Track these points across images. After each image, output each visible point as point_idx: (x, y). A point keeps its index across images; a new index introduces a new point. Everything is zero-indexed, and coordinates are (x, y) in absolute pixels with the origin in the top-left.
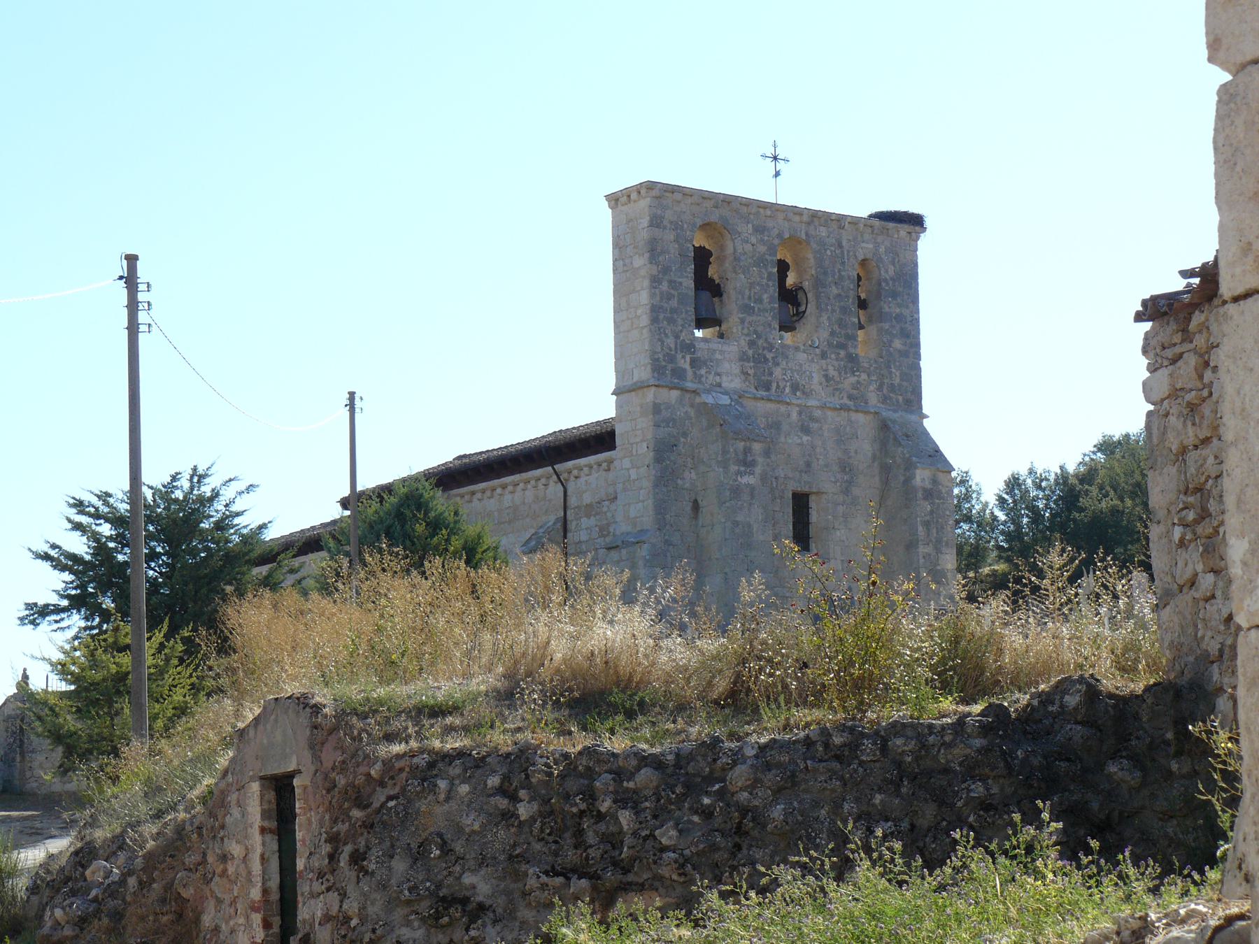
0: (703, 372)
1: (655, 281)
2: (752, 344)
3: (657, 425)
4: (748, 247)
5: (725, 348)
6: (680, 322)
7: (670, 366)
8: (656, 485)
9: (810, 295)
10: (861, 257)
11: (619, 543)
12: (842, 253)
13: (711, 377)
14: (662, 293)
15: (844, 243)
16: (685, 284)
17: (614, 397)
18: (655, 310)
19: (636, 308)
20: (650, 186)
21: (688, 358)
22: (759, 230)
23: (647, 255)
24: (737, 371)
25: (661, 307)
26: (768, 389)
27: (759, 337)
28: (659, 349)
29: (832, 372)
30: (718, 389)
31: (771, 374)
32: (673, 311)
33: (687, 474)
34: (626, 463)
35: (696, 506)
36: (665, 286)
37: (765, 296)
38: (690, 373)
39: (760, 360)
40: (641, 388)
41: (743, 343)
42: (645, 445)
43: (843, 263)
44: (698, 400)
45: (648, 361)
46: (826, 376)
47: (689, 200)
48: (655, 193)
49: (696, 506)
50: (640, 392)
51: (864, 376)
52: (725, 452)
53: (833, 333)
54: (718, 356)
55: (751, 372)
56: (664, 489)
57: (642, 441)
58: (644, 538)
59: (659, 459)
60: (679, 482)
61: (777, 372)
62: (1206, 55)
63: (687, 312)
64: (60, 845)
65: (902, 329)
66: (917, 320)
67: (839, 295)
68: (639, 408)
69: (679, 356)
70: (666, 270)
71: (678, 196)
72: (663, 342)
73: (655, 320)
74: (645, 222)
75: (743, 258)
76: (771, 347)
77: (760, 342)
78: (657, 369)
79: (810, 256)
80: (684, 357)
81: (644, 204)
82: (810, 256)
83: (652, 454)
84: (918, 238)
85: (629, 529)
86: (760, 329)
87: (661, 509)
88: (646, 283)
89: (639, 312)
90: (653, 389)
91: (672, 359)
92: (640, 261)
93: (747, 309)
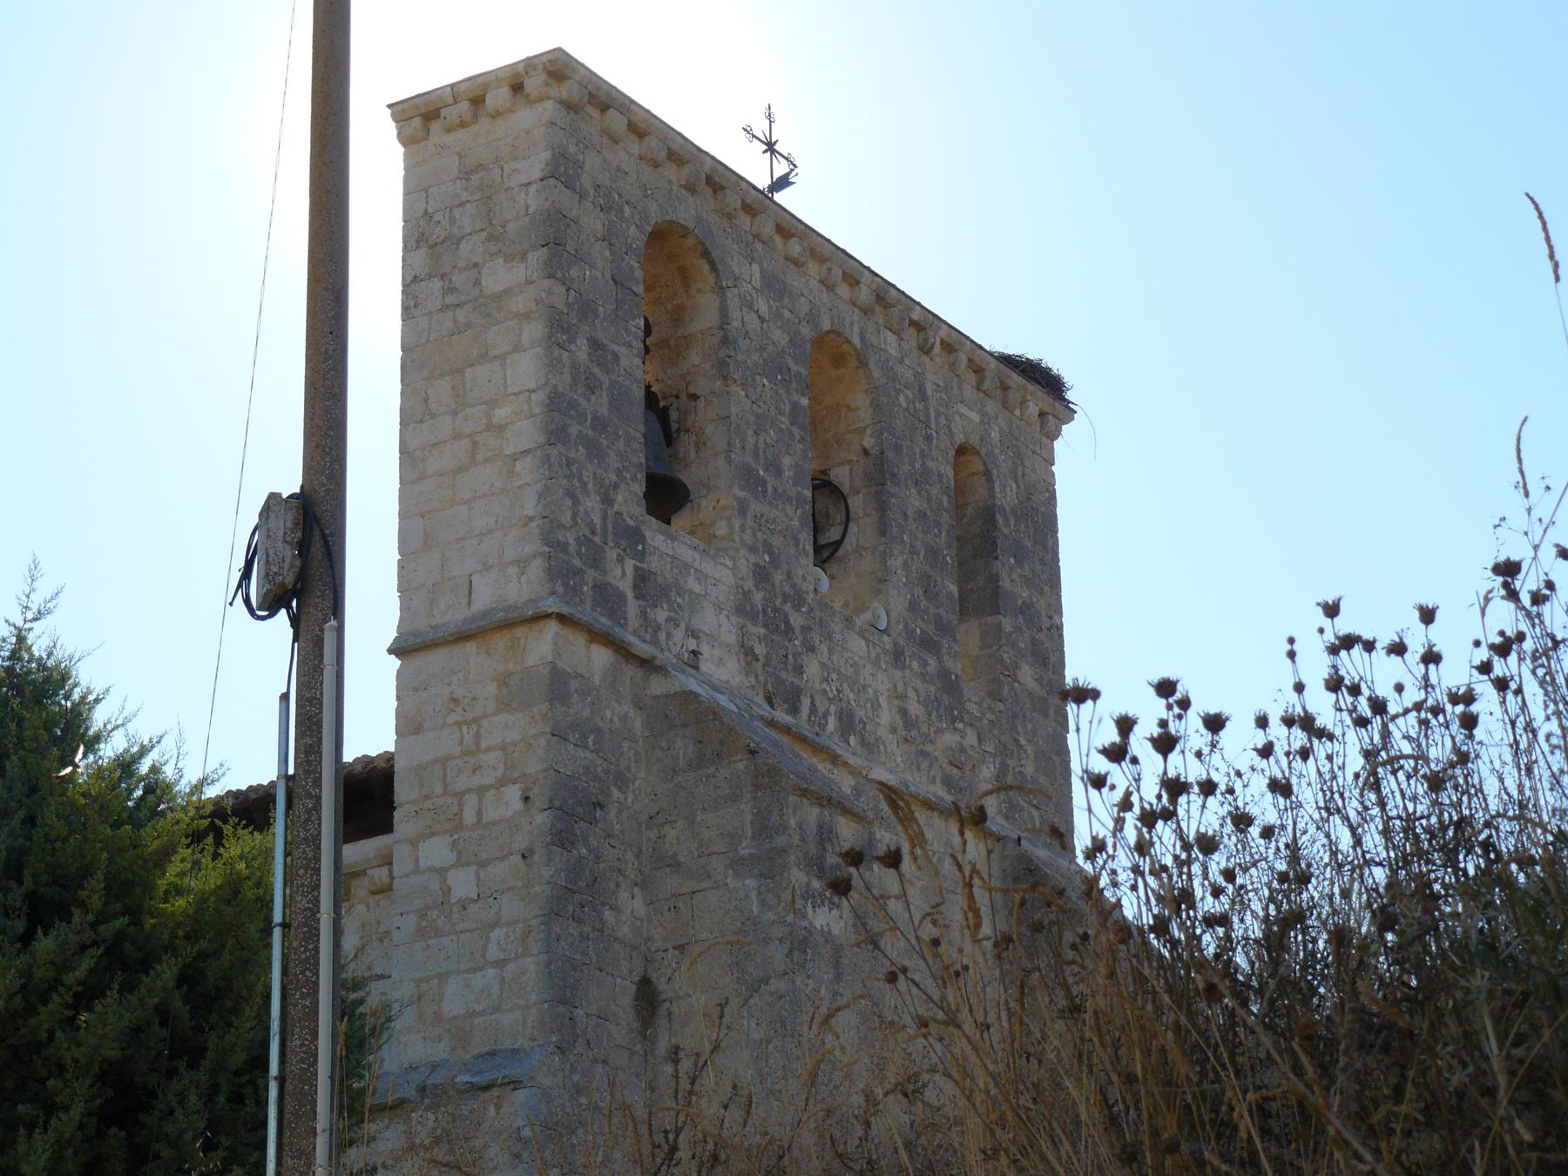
0: (661, 615)
1: (560, 328)
2: (762, 575)
3: (558, 734)
4: (753, 324)
5: (708, 567)
6: (613, 461)
7: (590, 575)
8: (552, 914)
9: (856, 502)
10: (960, 438)
11: (409, 1092)
12: (926, 409)
13: (679, 634)
14: (574, 366)
15: (929, 389)
16: (624, 362)
17: (395, 663)
18: (557, 404)
19: (492, 403)
20: (558, 68)
21: (630, 564)
22: (774, 286)
23: (537, 257)
24: (731, 638)
25: (573, 405)
26: (794, 711)
27: (775, 562)
28: (566, 519)
29: (915, 709)
30: (693, 672)
31: (799, 670)
32: (600, 424)
33: (623, 896)
34: (436, 851)
35: (648, 997)
36: (581, 350)
37: (787, 461)
38: (632, 608)
39: (778, 626)
40: (508, 625)
41: (744, 568)
42: (513, 794)
43: (928, 438)
44: (658, 686)
45: (534, 546)
46: (903, 712)
47: (635, 147)
48: (565, 90)
49: (648, 997)
50: (500, 641)
51: (971, 738)
52: (765, 828)
53: (913, 606)
54: (692, 583)
55: (760, 650)
56: (574, 929)
57: (501, 783)
58: (515, 1071)
59: (562, 838)
60: (608, 914)
61: (812, 669)
62: (1076, 463)
63: (629, 440)
64: (63, 773)
65: (1035, 643)
66: (1060, 628)
67: (922, 515)
68: (492, 689)
69: (612, 554)
70: (586, 309)
71: (617, 122)
72: (576, 503)
73: (556, 435)
74: (534, 166)
75: (742, 343)
76: (798, 600)
77: (778, 577)
78: (561, 573)
79: (861, 400)
80: (620, 560)
81: (532, 119)
82: (861, 400)
83: (541, 819)
84: (1056, 434)
85: (440, 1051)
86: (777, 541)
87: (564, 986)
88: (534, 331)
89: (501, 414)
90: (553, 627)
91: (596, 560)
92: (513, 278)
93: (750, 479)
